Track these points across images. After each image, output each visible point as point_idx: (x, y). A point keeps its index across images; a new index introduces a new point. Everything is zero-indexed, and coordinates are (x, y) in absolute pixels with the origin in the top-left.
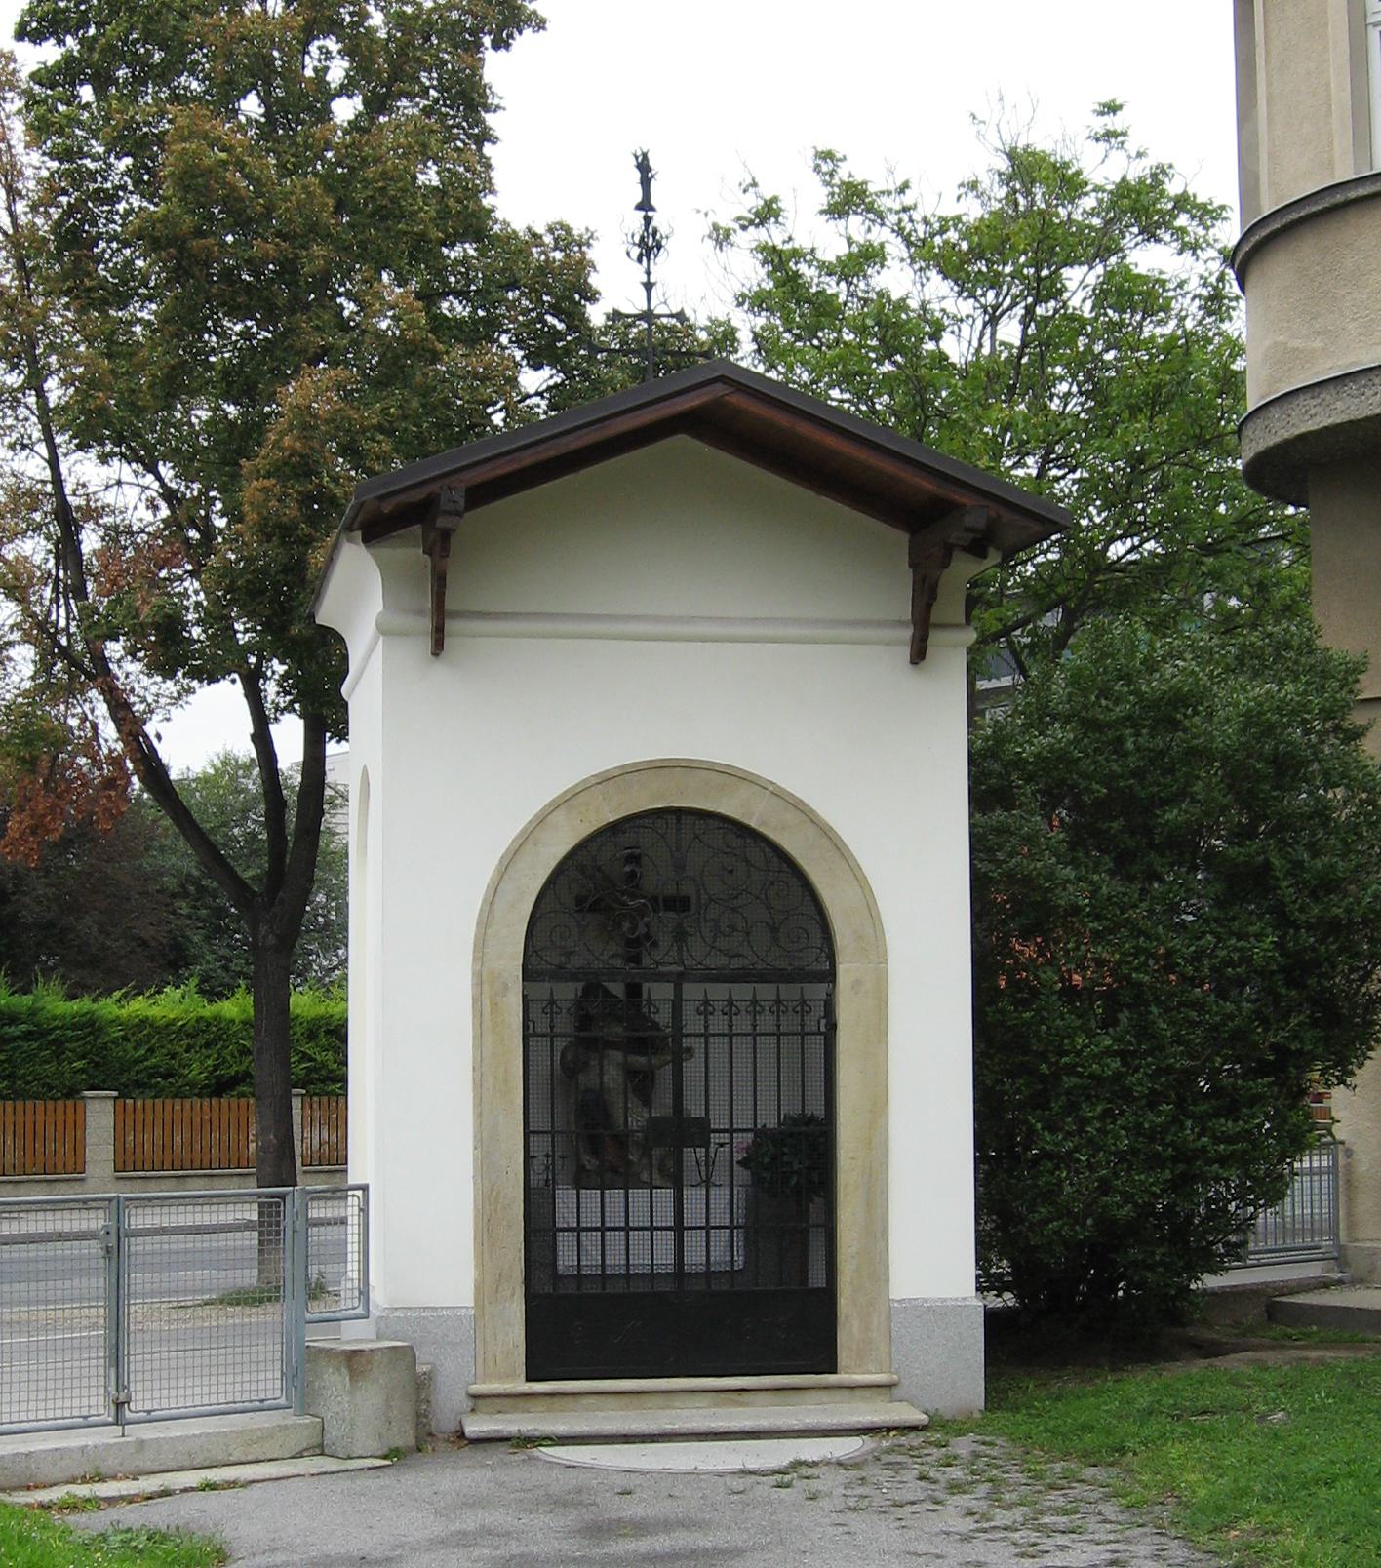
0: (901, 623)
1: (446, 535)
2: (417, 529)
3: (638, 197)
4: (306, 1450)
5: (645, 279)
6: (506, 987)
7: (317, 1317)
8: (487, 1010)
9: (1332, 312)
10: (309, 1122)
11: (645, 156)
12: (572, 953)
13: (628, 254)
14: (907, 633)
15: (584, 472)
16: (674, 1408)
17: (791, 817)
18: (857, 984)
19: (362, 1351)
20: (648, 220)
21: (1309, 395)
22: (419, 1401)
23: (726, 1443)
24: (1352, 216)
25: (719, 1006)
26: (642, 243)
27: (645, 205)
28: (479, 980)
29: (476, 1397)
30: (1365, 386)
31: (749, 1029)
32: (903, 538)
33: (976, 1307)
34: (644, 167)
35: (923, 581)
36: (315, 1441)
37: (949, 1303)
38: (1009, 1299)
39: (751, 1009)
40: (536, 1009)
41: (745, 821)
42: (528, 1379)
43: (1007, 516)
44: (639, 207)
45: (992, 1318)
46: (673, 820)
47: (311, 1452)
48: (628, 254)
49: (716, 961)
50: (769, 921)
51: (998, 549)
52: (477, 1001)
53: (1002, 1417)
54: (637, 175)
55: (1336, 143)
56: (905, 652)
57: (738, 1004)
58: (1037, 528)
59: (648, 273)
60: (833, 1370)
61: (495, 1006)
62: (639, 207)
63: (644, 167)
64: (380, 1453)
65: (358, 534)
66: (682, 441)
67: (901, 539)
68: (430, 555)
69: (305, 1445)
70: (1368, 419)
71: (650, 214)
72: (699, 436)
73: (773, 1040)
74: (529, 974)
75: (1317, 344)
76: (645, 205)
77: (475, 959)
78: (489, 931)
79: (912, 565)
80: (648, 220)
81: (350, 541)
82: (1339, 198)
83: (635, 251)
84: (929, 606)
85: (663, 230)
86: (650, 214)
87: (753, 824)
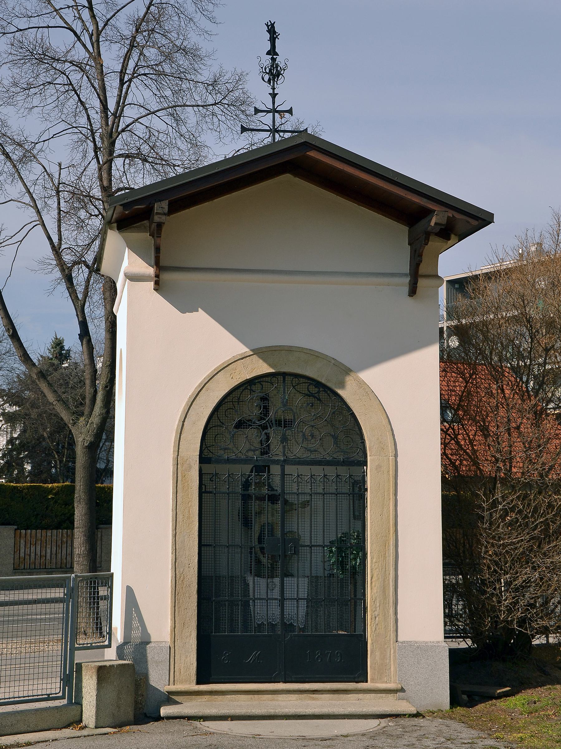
0: (405, 275)
1: (160, 226)
2: (146, 222)
3: (268, 47)
5: (271, 92)
6: (190, 467)
11: (273, 25)
13: (263, 79)
14: (407, 280)
15: (235, 194)
16: (278, 700)
18: (379, 467)
19: (105, 666)
20: (273, 60)
22: (136, 693)
23: (304, 721)
26: (270, 73)
27: (272, 52)
32: (406, 229)
33: (444, 647)
34: (272, 31)
35: (415, 251)
37: (429, 644)
38: (463, 644)
40: (206, 479)
41: (319, 379)
42: (199, 682)
43: (458, 216)
44: (268, 53)
45: (453, 653)
46: (281, 378)
48: (263, 79)
49: (305, 455)
51: (456, 235)
53: (460, 710)
54: (268, 36)
56: (406, 289)
58: (475, 223)
59: (274, 89)
62: (268, 53)
63: (272, 31)
64: (111, 726)
65: (115, 225)
66: (287, 177)
67: (403, 230)
68: (153, 237)
71: (275, 57)
72: (296, 175)
73: (334, 497)
76: (272, 52)
79: (410, 244)
80: (273, 60)
81: (111, 229)
83: (267, 77)
84: (418, 265)
85: (282, 65)
86: (275, 57)
87: (323, 381)
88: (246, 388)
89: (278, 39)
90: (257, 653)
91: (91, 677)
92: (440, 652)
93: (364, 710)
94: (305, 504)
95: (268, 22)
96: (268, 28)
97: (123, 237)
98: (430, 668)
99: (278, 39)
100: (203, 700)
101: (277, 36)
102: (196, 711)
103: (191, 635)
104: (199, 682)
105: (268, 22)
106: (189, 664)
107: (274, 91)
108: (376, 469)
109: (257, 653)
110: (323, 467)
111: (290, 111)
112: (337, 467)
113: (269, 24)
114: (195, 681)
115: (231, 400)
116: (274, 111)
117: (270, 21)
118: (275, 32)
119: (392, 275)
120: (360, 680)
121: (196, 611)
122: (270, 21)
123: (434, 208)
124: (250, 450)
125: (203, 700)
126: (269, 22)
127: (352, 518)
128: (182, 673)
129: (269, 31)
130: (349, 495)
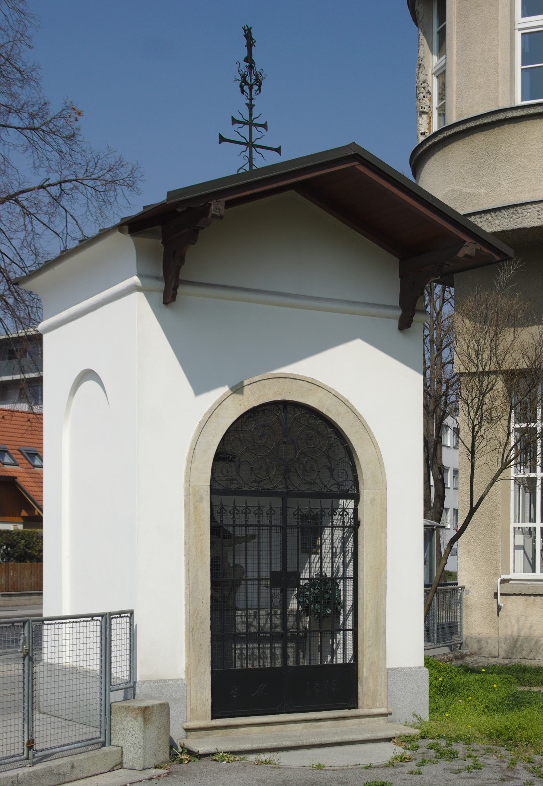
0: (394, 308)
2: (159, 228)
3: (246, 54)
4: (115, 766)
5: (248, 102)
6: (201, 498)
7: (115, 688)
8: (192, 510)
9: (493, 175)
10: (439, 608)
11: (249, 30)
12: (232, 479)
17: (342, 409)
18: (373, 500)
21: (479, 216)
24: (507, 128)
25: (228, 509)
28: (187, 494)
29: (187, 730)
30: (513, 213)
31: (232, 523)
34: (248, 34)
36: (118, 761)
39: (257, 512)
42: (214, 717)
44: (246, 60)
47: (117, 767)
50: (329, 465)
52: (187, 505)
54: (245, 41)
55: (500, 88)
57: (347, 510)
60: (356, 707)
61: (196, 508)
63: (248, 34)
69: (114, 764)
70: (513, 231)
74: (213, 492)
75: (483, 191)
76: (249, 59)
77: (186, 481)
78: (192, 465)
82: (501, 116)
87: (324, 411)
88: (249, 417)
89: (255, 46)
90: (262, 686)
91: (135, 718)
92: (422, 676)
93: (379, 735)
94: (248, 538)
95: (245, 27)
96: (245, 33)
97: (136, 245)
98: (414, 691)
99: (255, 46)
100: (219, 735)
101: (253, 44)
102: (231, 746)
103: (205, 671)
104: (214, 717)
105: (245, 27)
106: (205, 700)
107: (251, 102)
108: (371, 502)
109: (262, 686)
110: (308, 499)
111: (265, 126)
112: (334, 500)
113: (246, 28)
114: (210, 716)
115: (236, 429)
116: (250, 123)
117: (247, 25)
118: (252, 39)
119: (385, 306)
120: (352, 706)
121: (210, 647)
122: (247, 25)
123: (466, 240)
124: (254, 481)
125: (219, 735)
126: (246, 27)
127: (300, 551)
128: (198, 710)
129: (246, 36)
130: (298, 528)
